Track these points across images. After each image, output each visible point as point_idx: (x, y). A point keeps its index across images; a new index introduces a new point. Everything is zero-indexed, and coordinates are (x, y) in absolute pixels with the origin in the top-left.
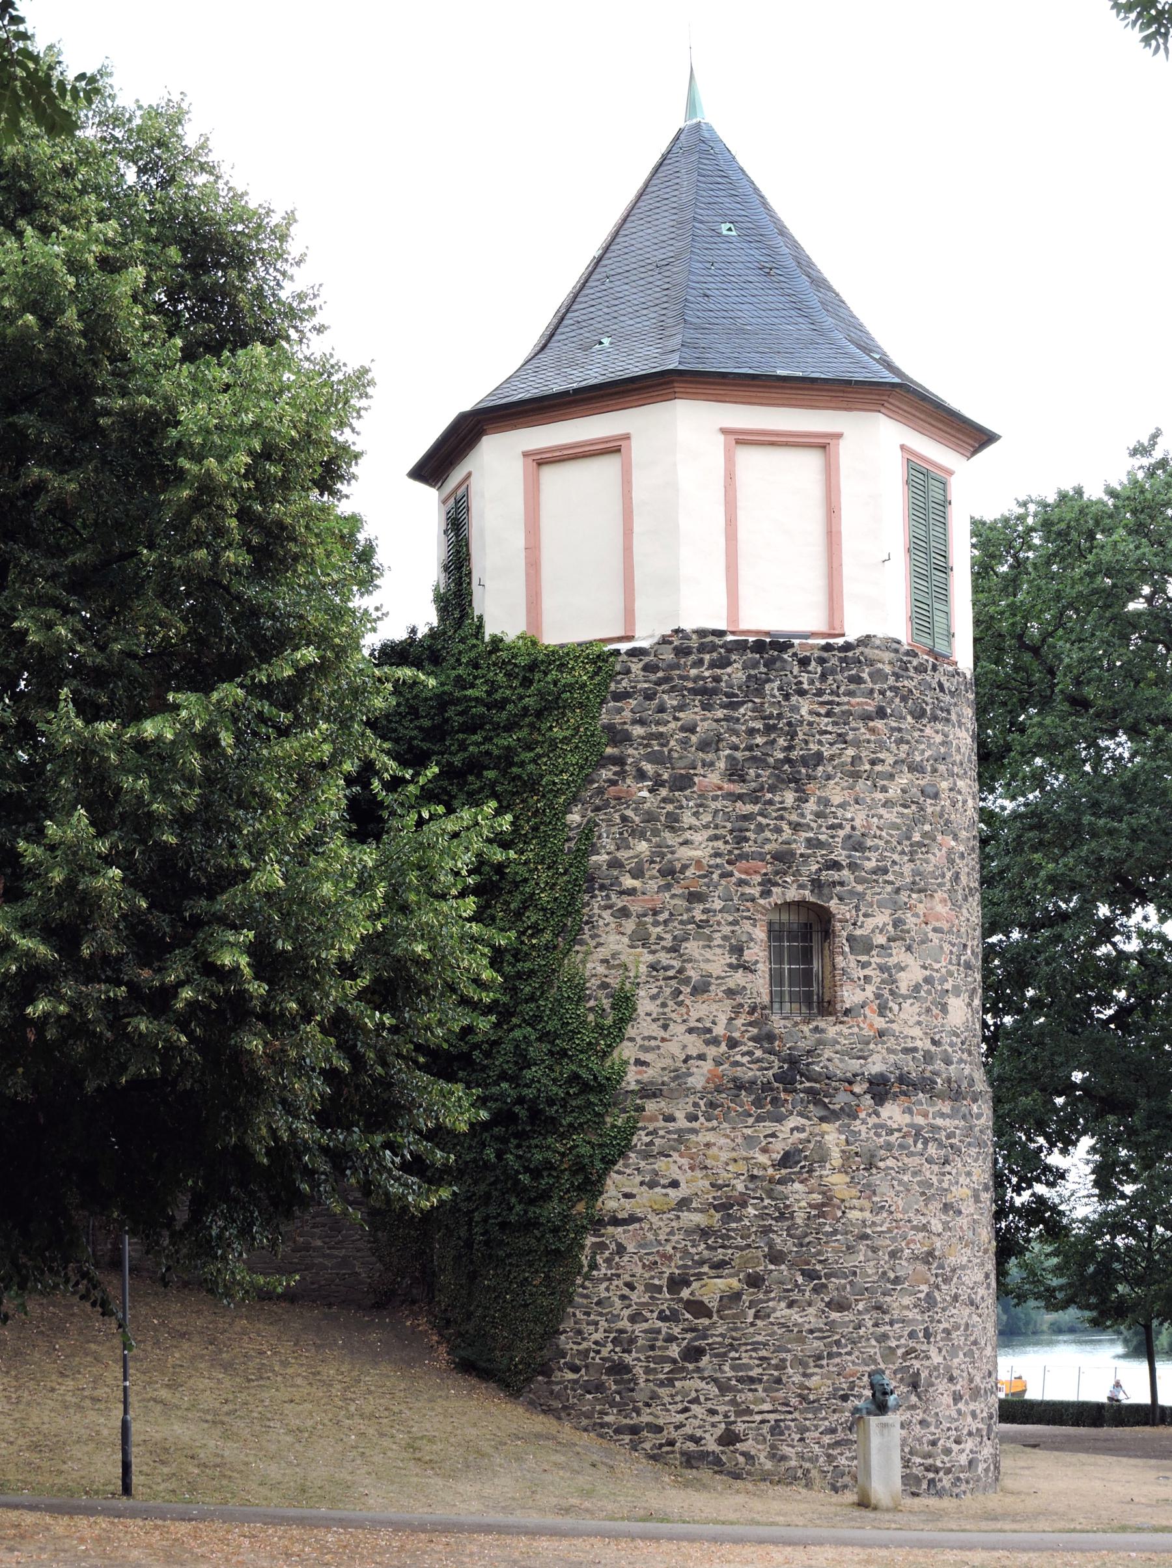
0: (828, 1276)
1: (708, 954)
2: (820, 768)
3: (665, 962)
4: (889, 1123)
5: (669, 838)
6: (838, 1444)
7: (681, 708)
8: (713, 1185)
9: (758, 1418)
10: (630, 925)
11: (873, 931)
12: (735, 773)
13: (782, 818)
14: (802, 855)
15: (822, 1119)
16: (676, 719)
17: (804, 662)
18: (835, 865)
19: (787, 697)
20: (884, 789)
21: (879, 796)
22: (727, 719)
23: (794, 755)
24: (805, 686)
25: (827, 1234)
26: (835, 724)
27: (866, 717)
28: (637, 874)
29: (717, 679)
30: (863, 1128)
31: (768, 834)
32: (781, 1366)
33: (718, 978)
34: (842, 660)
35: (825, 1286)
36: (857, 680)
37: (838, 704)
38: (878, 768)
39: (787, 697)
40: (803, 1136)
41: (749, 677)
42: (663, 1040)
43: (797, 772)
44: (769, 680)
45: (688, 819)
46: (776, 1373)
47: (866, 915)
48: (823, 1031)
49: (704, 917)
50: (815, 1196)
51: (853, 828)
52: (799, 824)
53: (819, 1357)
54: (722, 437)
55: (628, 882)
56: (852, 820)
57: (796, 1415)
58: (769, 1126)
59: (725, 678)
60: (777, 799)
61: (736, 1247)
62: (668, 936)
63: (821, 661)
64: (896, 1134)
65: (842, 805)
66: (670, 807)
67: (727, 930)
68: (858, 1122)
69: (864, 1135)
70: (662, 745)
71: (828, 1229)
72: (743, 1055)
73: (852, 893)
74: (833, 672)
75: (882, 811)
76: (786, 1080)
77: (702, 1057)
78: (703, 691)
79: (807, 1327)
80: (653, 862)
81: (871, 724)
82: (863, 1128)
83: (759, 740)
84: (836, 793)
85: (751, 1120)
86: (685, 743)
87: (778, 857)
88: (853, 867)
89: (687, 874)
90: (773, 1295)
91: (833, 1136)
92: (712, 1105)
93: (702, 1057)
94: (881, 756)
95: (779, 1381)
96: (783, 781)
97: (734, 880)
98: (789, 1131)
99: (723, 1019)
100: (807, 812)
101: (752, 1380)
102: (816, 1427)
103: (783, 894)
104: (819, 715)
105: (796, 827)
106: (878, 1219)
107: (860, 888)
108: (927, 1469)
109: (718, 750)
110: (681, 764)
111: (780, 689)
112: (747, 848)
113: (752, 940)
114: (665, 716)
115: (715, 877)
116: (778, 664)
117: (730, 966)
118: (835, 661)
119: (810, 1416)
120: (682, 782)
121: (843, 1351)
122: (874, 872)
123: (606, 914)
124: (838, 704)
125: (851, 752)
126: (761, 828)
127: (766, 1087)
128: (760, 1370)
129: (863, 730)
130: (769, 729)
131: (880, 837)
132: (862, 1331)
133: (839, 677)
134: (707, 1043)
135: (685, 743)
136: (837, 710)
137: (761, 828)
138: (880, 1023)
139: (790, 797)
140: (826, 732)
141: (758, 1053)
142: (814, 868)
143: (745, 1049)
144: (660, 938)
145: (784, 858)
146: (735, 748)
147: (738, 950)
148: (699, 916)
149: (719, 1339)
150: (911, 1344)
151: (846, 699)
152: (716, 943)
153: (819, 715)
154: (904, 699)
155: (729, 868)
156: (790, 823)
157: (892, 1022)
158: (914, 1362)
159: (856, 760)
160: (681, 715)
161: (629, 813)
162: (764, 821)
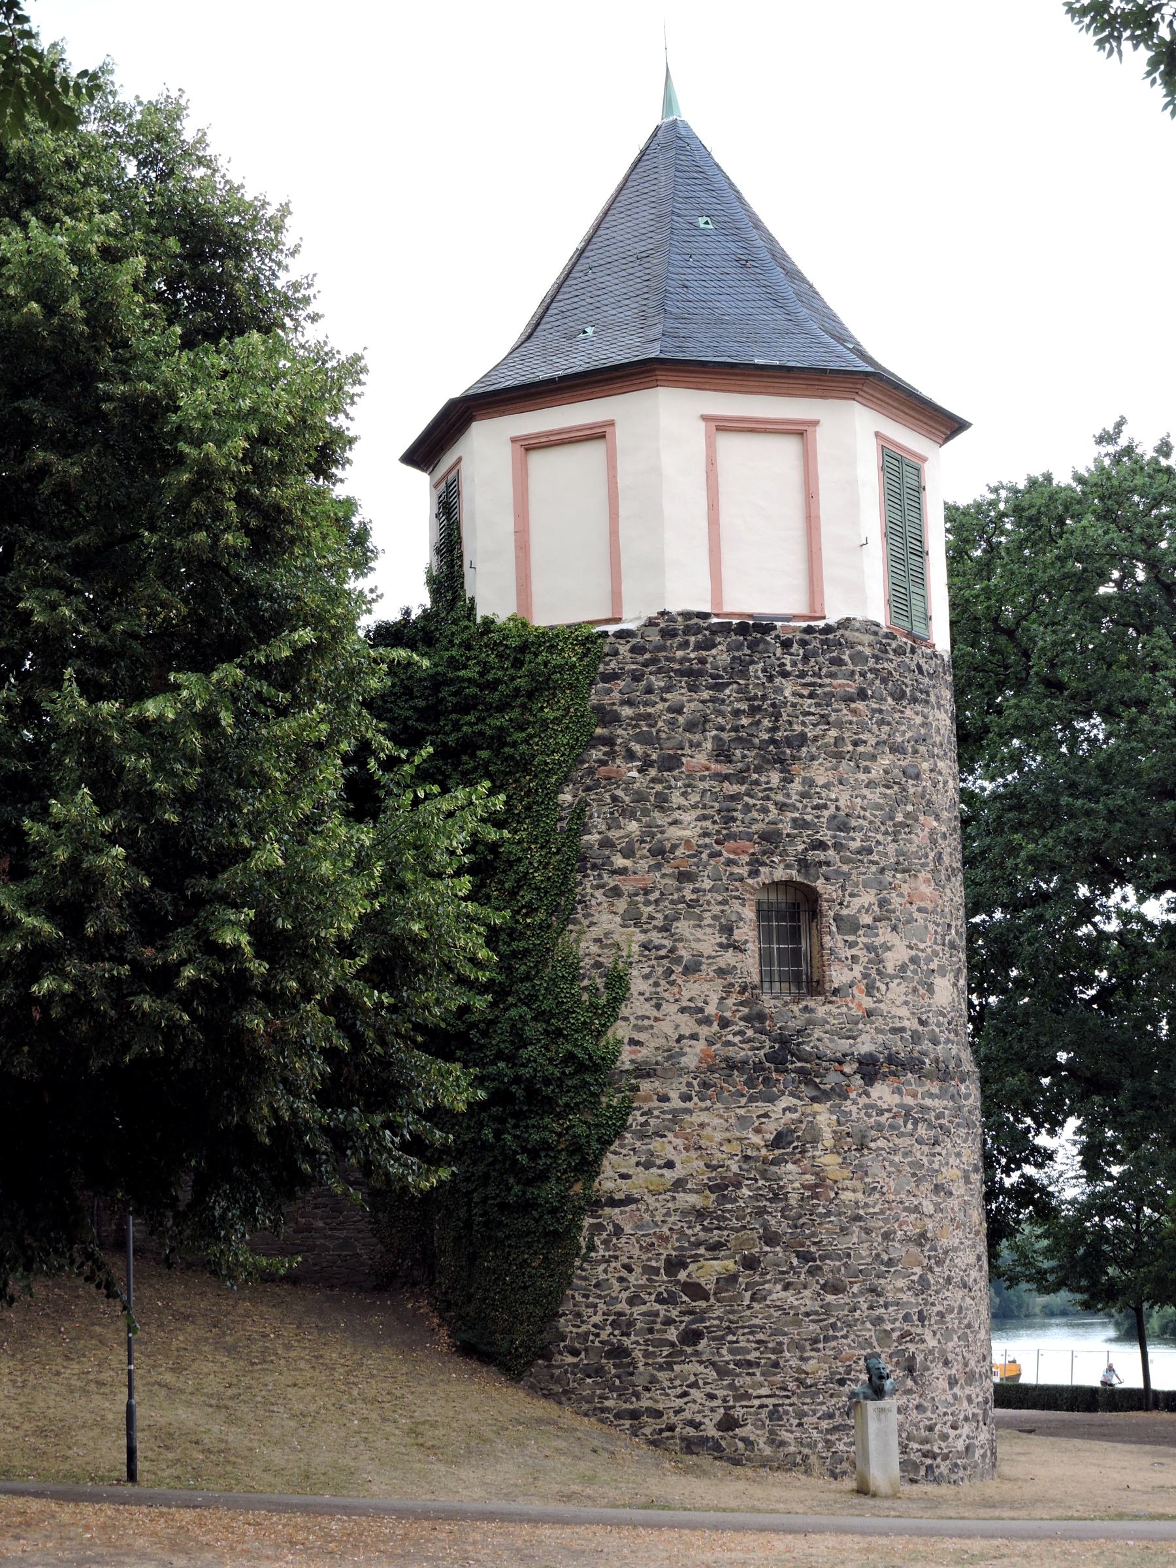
1: (699, 933)
2: (804, 749)
3: (657, 942)
4: (879, 1103)
5: (659, 818)
6: (835, 1429)
7: (668, 689)
8: (707, 1166)
9: (756, 1402)
10: (622, 905)
11: (859, 911)
12: (722, 753)
13: (768, 798)
14: (788, 835)
15: (813, 1099)
16: (664, 700)
17: (786, 644)
18: (821, 845)
19: (770, 678)
20: (867, 770)
22: (713, 700)
23: (779, 735)
26: (818, 705)
27: (848, 699)
28: (628, 853)
29: (702, 661)
30: (854, 1109)
31: (755, 814)
32: (778, 1350)
33: (709, 957)
35: (819, 1268)
36: (839, 662)
37: (821, 686)
39: (770, 678)
40: (795, 1116)
41: (734, 658)
42: (656, 1019)
43: (782, 753)
45: (676, 799)
46: (773, 1357)
48: (812, 1011)
49: (694, 897)
50: (808, 1177)
51: (838, 808)
52: (784, 805)
53: (815, 1341)
55: (620, 862)
56: (837, 800)
57: (794, 1399)
58: (761, 1107)
60: (763, 779)
61: (732, 1229)
62: (659, 916)
63: (803, 643)
64: (887, 1115)
65: (826, 786)
67: (716, 909)
68: (849, 1102)
70: (650, 726)
71: (821, 1210)
72: (735, 1034)
73: (838, 872)
74: (815, 655)
75: (865, 792)
76: (778, 1059)
77: (694, 1037)
78: (689, 673)
79: (803, 1309)
81: (853, 705)
82: (854, 1109)
85: (743, 1101)
86: (672, 723)
87: (765, 837)
88: (838, 846)
90: (768, 1277)
91: (824, 1116)
92: (705, 1085)
93: (694, 1037)
95: (776, 1365)
96: (768, 762)
97: (722, 859)
99: (714, 999)
100: (792, 792)
101: (750, 1364)
102: (814, 1412)
104: (802, 696)
105: (782, 807)
106: (870, 1200)
107: (845, 868)
109: (704, 731)
110: (669, 744)
111: (764, 670)
112: (735, 828)
113: (741, 919)
114: (652, 697)
115: (704, 856)
117: (721, 945)
119: (808, 1400)
120: (671, 763)
123: (599, 893)
124: (821, 686)
125: (833, 733)
126: (748, 808)
127: (759, 1067)
128: (757, 1354)
130: (754, 710)
133: (821, 659)
134: (700, 1022)
136: (819, 691)
137: (748, 808)
141: (750, 1033)
142: (801, 847)
143: (736, 1028)
144: (651, 917)
145: (770, 838)
147: (728, 929)
149: (716, 1322)
152: (706, 922)
153: (802, 696)
154: (884, 681)
155: (718, 848)
156: (776, 804)
158: (909, 1345)
159: (839, 740)
162: (751, 801)
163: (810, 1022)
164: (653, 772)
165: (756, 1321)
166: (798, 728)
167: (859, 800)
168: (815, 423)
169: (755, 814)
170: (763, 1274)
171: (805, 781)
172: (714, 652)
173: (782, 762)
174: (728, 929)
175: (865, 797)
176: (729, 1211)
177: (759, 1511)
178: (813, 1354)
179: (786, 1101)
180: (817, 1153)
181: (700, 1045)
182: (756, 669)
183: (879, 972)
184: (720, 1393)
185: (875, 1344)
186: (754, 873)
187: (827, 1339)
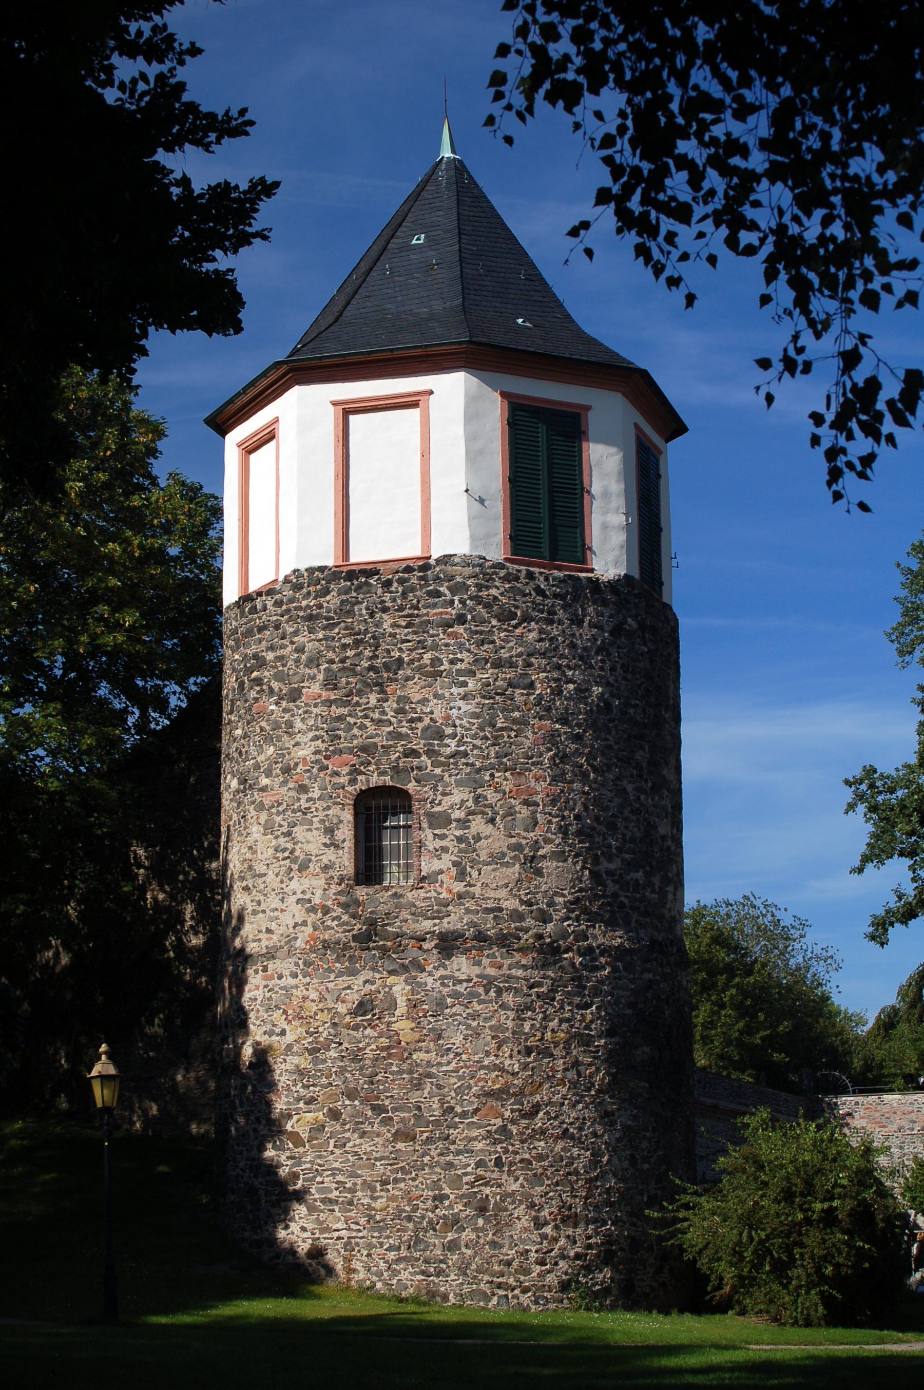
1: (309, 836)
3: (283, 845)
4: (457, 974)
5: (287, 742)
6: (399, 1260)
7: (296, 633)
8: (307, 1032)
9: (336, 1234)
10: (264, 817)
12: (331, 683)
13: (366, 717)
14: (383, 746)
16: (292, 643)
17: (387, 584)
18: (414, 753)
19: (372, 615)
22: (326, 638)
25: (392, 1073)
26: (415, 633)
28: (268, 774)
29: (320, 606)
30: (430, 980)
31: (355, 731)
32: (353, 1191)
33: (317, 856)
35: (391, 1119)
37: (418, 616)
38: (459, 666)
39: (372, 615)
40: (373, 988)
41: (342, 602)
42: (282, 911)
44: (358, 603)
45: (298, 725)
46: (349, 1196)
47: (444, 794)
48: (401, 896)
49: (307, 805)
52: (380, 721)
54: (332, 408)
55: (264, 781)
56: (432, 713)
57: (364, 1233)
58: (344, 981)
59: (325, 605)
61: (321, 1086)
62: (285, 824)
63: (401, 581)
64: (465, 985)
66: (287, 716)
67: (321, 814)
69: (429, 985)
70: (284, 666)
71: (394, 1068)
72: (333, 920)
73: (432, 776)
74: (413, 589)
75: (461, 703)
76: (364, 939)
77: (305, 923)
78: (310, 618)
80: (276, 763)
83: (350, 653)
85: (332, 976)
86: (297, 661)
87: (364, 749)
88: (430, 753)
89: (298, 770)
90: (347, 1127)
91: (400, 988)
92: (307, 964)
93: (305, 923)
95: (351, 1203)
96: (368, 685)
97: (329, 772)
99: (319, 893)
101: (331, 1201)
102: (381, 1244)
103: (368, 781)
104: (399, 626)
105: (379, 723)
106: (444, 1060)
107: (438, 771)
108: (499, 1286)
109: (318, 665)
110: (296, 679)
111: (367, 608)
113: (341, 822)
114: (284, 641)
115: (315, 770)
116: (365, 589)
117: (325, 845)
118: (414, 580)
119: (376, 1234)
120: (295, 695)
121: (408, 1177)
122: (453, 755)
123: (252, 808)
124: (418, 616)
125: (427, 657)
126: (350, 727)
127: (346, 947)
128: (336, 1193)
129: (441, 636)
130: (357, 643)
132: (426, 1159)
133: (418, 593)
134: (308, 911)
135: (297, 661)
137: (350, 727)
139: (373, 699)
141: (345, 918)
143: (334, 914)
144: (280, 826)
146: (332, 662)
147: (330, 831)
148: (304, 804)
149: (309, 1166)
150: (480, 1172)
151: (425, 611)
152: (315, 826)
153: (399, 626)
154: (488, 606)
155: (326, 762)
156: (372, 720)
158: (482, 1188)
159: (436, 661)
160: (296, 639)
161: (263, 724)
162: (351, 720)
163: (398, 906)
164: (284, 704)
165: (336, 1165)
166: (396, 654)
168: (588, 408)
169: (355, 731)
170: (344, 1124)
171: (400, 699)
172: (328, 598)
174: (330, 831)
176: (320, 1070)
178: (382, 1193)
179: (367, 974)
181: (309, 930)
182: (362, 610)
184: (309, 1226)
186: (353, 781)
187: (396, 1181)
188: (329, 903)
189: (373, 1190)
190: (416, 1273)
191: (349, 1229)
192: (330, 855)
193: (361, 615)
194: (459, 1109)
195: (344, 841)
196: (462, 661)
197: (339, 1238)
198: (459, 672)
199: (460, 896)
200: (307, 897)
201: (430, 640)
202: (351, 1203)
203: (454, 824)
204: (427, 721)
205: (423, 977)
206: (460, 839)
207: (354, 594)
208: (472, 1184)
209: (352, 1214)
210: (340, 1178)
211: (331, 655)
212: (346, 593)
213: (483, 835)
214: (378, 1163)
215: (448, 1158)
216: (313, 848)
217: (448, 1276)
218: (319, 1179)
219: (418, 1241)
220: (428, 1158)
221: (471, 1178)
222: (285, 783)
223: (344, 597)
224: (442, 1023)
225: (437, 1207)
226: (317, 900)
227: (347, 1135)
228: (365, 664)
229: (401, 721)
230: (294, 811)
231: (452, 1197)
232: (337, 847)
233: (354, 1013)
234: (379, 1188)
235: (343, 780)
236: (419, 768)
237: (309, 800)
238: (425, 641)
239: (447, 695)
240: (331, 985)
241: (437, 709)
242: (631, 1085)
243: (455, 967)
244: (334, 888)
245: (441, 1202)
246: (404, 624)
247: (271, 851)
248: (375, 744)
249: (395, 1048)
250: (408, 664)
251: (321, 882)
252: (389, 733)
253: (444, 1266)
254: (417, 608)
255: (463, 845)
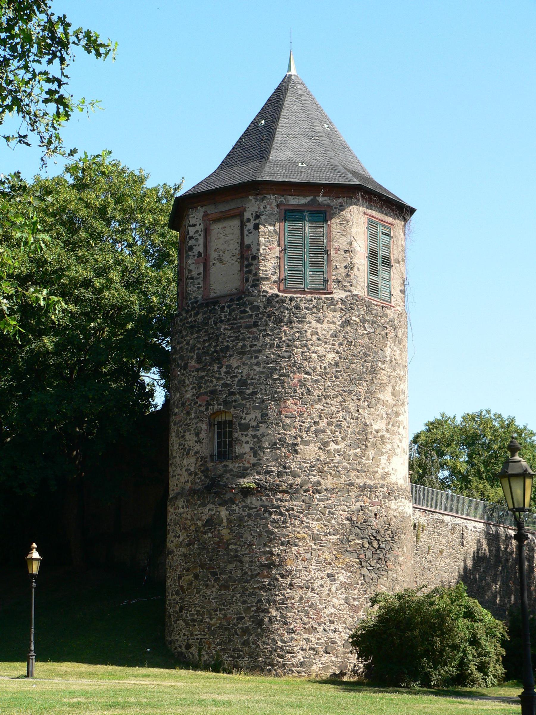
0: (221, 574)
2: (228, 353)
9: (196, 637)
11: (250, 420)
13: (212, 376)
14: (220, 391)
15: (220, 505)
18: (232, 394)
19: (216, 325)
20: (257, 357)
21: (254, 361)
22: (198, 337)
23: (218, 348)
24: (223, 319)
25: (220, 555)
26: (234, 332)
27: (248, 327)
30: (237, 508)
32: (203, 615)
34: (237, 305)
35: (218, 578)
36: (245, 312)
37: (236, 324)
39: (216, 325)
43: (219, 356)
45: (187, 381)
47: (247, 414)
48: (227, 466)
50: (216, 539)
51: (242, 376)
53: (216, 611)
56: (242, 372)
58: (200, 510)
60: (212, 368)
64: (254, 510)
65: (237, 368)
68: (235, 505)
69: (237, 511)
75: (255, 367)
76: (209, 488)
77: (188, 481)
79: (212, 597)
81: (250, 330)
82: (237, 508)
84: (234, 362)
85: (196, 507)
88: (241, 393)
91: (224, 513)
93: (188, 481)
94: (255, 343)
98: (206, 512)
99: (193, 465)
100: (222, 372)
105: (218, 379)
107: (244, 402)
109: (194, 351)
111: (214, 321)
112: (202, 391)
115: (192, 404)
117: (196, 441)
119: (212, 637)
120: (185, 367)
121: (225, 608)
124: (236, 324)
125: (241, 344)
126: (206, 381)
130: (210, 339)
131: (255, 379)
132: (234, 599)
133: (236, 312)
136: (235, 326)
138: (253, 460)
140: (231, 337)
142: (224, 396)
145: (213, 392)
146: (199, 349)
147: (197, 435)
148: (189, 422)
157: (260, 460)
159: (244, 346)
166: (226, 344)
167: (252, 371)
173: (218, 359)
174: (197, 435)
175: (255, 370)
177: (459, 702)
179: (211, 506)
180: (220, 529)
182: (212, 321)
183: (259, 447)
185: (243, 612)
186: (207, 409)
188: (197, 471)
189: (211, 614)
190: (229, 657)
191: (201, 634)
192: (198, 447)
193: (211, 325)
194: (250, 573)
195: (203, 439)
196: (256, 345)
197: (197, 639)
198: (255, 351)
199: (254, 465)
200: (189, 468)
201: (241, 336)
202: (201, 621)
203: (251, 429)
204: (240, 377)
205: (235, 507)
206: (254, 436)
207: (209, 314)
208: (256, 611)
209: (202, 627)
210: (198, 608)
211: (199, 346)
212: (205, 314)
213: (266, 434)
214: (213, 601)
215: (244, 599)
216: (191, 443)
217: (244, 658)
218: (190, 609)
219: (230, 640)
220: (235, 598)
221: (255, 608)
222: (182, 411)
223: (205, 316)
224: (242, 531)
225: (238, 623)
226: (192, 470)
227: (201, 587)
228: (213, 350)
229: (227, 377)
230: (185, 425)
231: (246, 618)
232: (200, 442)
233: (204, 526)
234: (213, 613)
235: (203, 409)
236: (235, 401)
237: (190, 419)
238: (239, 336)
239: (249, 363)
240: (196, 512)
241: (244, 371)
242: (347, 560)
243: (249, 501)
244: (199, 463)
245: (241, 621)
246: (229, 328)
247: (178, 445)
248: (216, 390)
249: (222, 544)
250: (231, 349)
251: (193, 460)
252: (223, 384)
253: (241, 653)
254: (235, 320)
255: (256, 440)
